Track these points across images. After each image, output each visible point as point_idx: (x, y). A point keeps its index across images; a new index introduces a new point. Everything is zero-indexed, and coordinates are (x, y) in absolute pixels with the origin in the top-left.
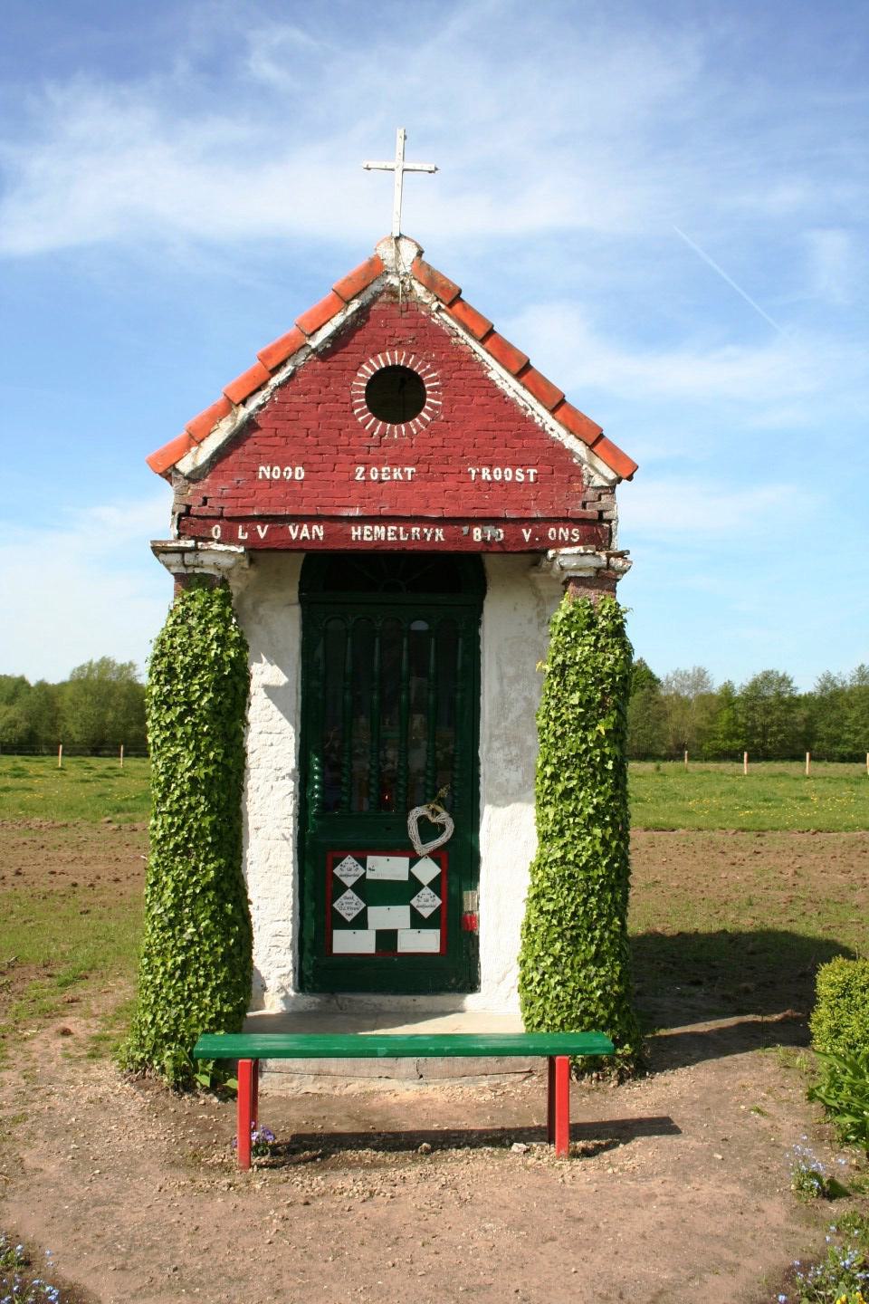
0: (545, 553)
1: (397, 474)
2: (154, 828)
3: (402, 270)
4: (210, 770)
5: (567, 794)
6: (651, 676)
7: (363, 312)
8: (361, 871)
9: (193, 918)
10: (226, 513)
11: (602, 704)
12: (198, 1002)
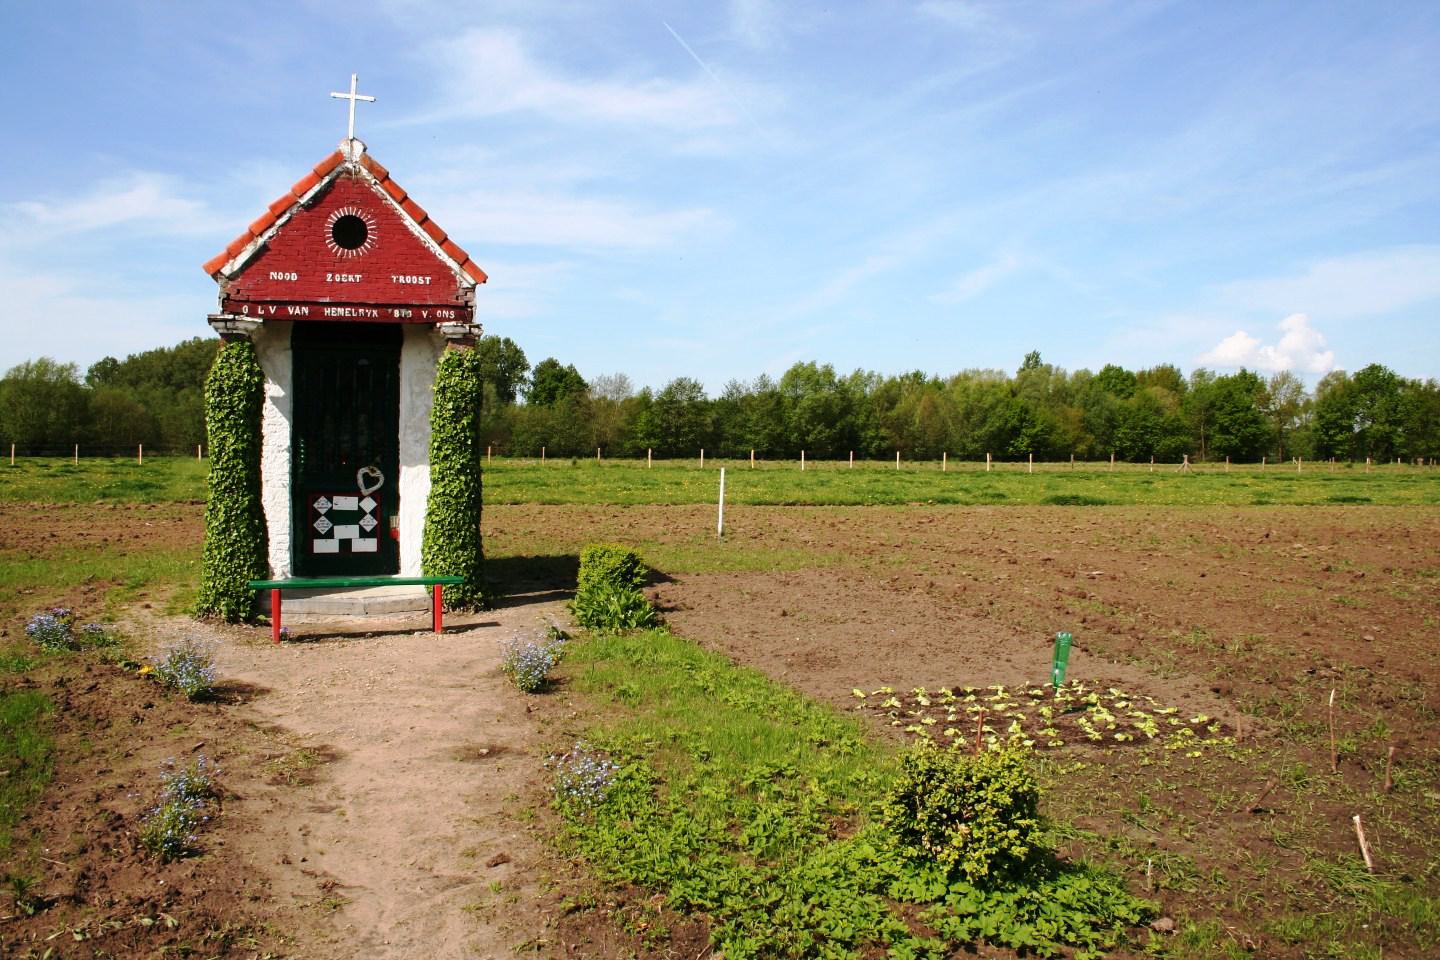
0: (435, 324)
1: (351, 278)
2: (212, 478)
3: (354, 159)
4: (245, 445)
5: (446, 457)
6: (580, 381)
7: (331, 183)
8: (330, 505)
9: (236, 528)
10: (251, 299)
11: (465, 408)
12: (240, 574)
